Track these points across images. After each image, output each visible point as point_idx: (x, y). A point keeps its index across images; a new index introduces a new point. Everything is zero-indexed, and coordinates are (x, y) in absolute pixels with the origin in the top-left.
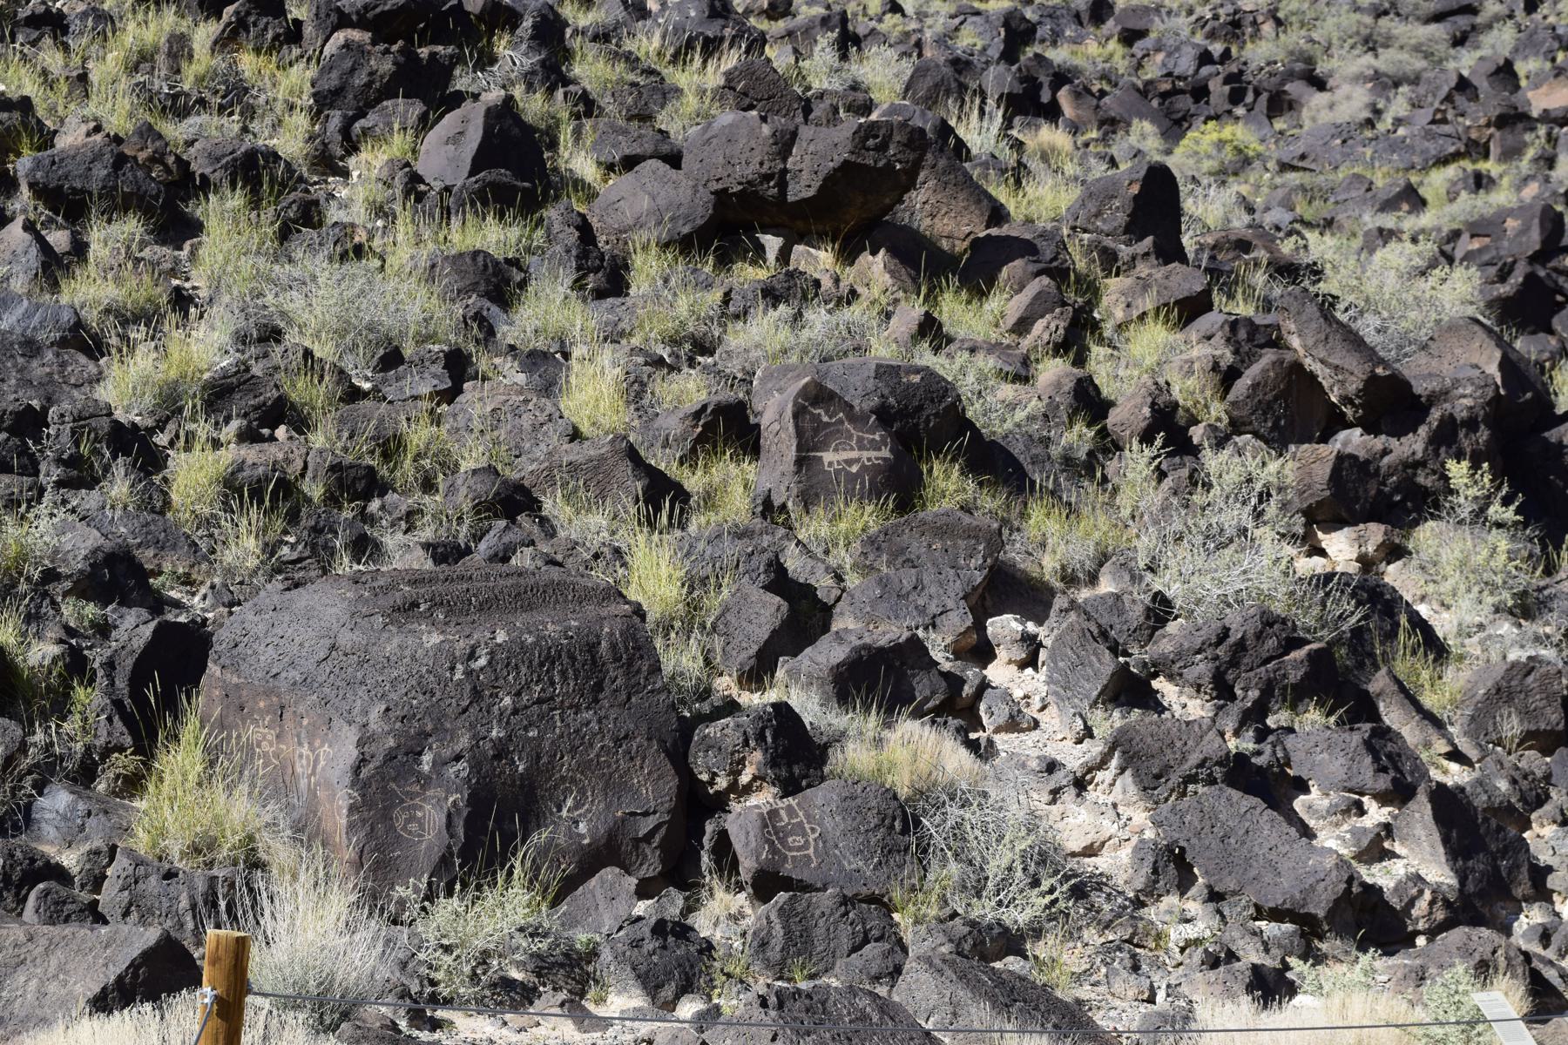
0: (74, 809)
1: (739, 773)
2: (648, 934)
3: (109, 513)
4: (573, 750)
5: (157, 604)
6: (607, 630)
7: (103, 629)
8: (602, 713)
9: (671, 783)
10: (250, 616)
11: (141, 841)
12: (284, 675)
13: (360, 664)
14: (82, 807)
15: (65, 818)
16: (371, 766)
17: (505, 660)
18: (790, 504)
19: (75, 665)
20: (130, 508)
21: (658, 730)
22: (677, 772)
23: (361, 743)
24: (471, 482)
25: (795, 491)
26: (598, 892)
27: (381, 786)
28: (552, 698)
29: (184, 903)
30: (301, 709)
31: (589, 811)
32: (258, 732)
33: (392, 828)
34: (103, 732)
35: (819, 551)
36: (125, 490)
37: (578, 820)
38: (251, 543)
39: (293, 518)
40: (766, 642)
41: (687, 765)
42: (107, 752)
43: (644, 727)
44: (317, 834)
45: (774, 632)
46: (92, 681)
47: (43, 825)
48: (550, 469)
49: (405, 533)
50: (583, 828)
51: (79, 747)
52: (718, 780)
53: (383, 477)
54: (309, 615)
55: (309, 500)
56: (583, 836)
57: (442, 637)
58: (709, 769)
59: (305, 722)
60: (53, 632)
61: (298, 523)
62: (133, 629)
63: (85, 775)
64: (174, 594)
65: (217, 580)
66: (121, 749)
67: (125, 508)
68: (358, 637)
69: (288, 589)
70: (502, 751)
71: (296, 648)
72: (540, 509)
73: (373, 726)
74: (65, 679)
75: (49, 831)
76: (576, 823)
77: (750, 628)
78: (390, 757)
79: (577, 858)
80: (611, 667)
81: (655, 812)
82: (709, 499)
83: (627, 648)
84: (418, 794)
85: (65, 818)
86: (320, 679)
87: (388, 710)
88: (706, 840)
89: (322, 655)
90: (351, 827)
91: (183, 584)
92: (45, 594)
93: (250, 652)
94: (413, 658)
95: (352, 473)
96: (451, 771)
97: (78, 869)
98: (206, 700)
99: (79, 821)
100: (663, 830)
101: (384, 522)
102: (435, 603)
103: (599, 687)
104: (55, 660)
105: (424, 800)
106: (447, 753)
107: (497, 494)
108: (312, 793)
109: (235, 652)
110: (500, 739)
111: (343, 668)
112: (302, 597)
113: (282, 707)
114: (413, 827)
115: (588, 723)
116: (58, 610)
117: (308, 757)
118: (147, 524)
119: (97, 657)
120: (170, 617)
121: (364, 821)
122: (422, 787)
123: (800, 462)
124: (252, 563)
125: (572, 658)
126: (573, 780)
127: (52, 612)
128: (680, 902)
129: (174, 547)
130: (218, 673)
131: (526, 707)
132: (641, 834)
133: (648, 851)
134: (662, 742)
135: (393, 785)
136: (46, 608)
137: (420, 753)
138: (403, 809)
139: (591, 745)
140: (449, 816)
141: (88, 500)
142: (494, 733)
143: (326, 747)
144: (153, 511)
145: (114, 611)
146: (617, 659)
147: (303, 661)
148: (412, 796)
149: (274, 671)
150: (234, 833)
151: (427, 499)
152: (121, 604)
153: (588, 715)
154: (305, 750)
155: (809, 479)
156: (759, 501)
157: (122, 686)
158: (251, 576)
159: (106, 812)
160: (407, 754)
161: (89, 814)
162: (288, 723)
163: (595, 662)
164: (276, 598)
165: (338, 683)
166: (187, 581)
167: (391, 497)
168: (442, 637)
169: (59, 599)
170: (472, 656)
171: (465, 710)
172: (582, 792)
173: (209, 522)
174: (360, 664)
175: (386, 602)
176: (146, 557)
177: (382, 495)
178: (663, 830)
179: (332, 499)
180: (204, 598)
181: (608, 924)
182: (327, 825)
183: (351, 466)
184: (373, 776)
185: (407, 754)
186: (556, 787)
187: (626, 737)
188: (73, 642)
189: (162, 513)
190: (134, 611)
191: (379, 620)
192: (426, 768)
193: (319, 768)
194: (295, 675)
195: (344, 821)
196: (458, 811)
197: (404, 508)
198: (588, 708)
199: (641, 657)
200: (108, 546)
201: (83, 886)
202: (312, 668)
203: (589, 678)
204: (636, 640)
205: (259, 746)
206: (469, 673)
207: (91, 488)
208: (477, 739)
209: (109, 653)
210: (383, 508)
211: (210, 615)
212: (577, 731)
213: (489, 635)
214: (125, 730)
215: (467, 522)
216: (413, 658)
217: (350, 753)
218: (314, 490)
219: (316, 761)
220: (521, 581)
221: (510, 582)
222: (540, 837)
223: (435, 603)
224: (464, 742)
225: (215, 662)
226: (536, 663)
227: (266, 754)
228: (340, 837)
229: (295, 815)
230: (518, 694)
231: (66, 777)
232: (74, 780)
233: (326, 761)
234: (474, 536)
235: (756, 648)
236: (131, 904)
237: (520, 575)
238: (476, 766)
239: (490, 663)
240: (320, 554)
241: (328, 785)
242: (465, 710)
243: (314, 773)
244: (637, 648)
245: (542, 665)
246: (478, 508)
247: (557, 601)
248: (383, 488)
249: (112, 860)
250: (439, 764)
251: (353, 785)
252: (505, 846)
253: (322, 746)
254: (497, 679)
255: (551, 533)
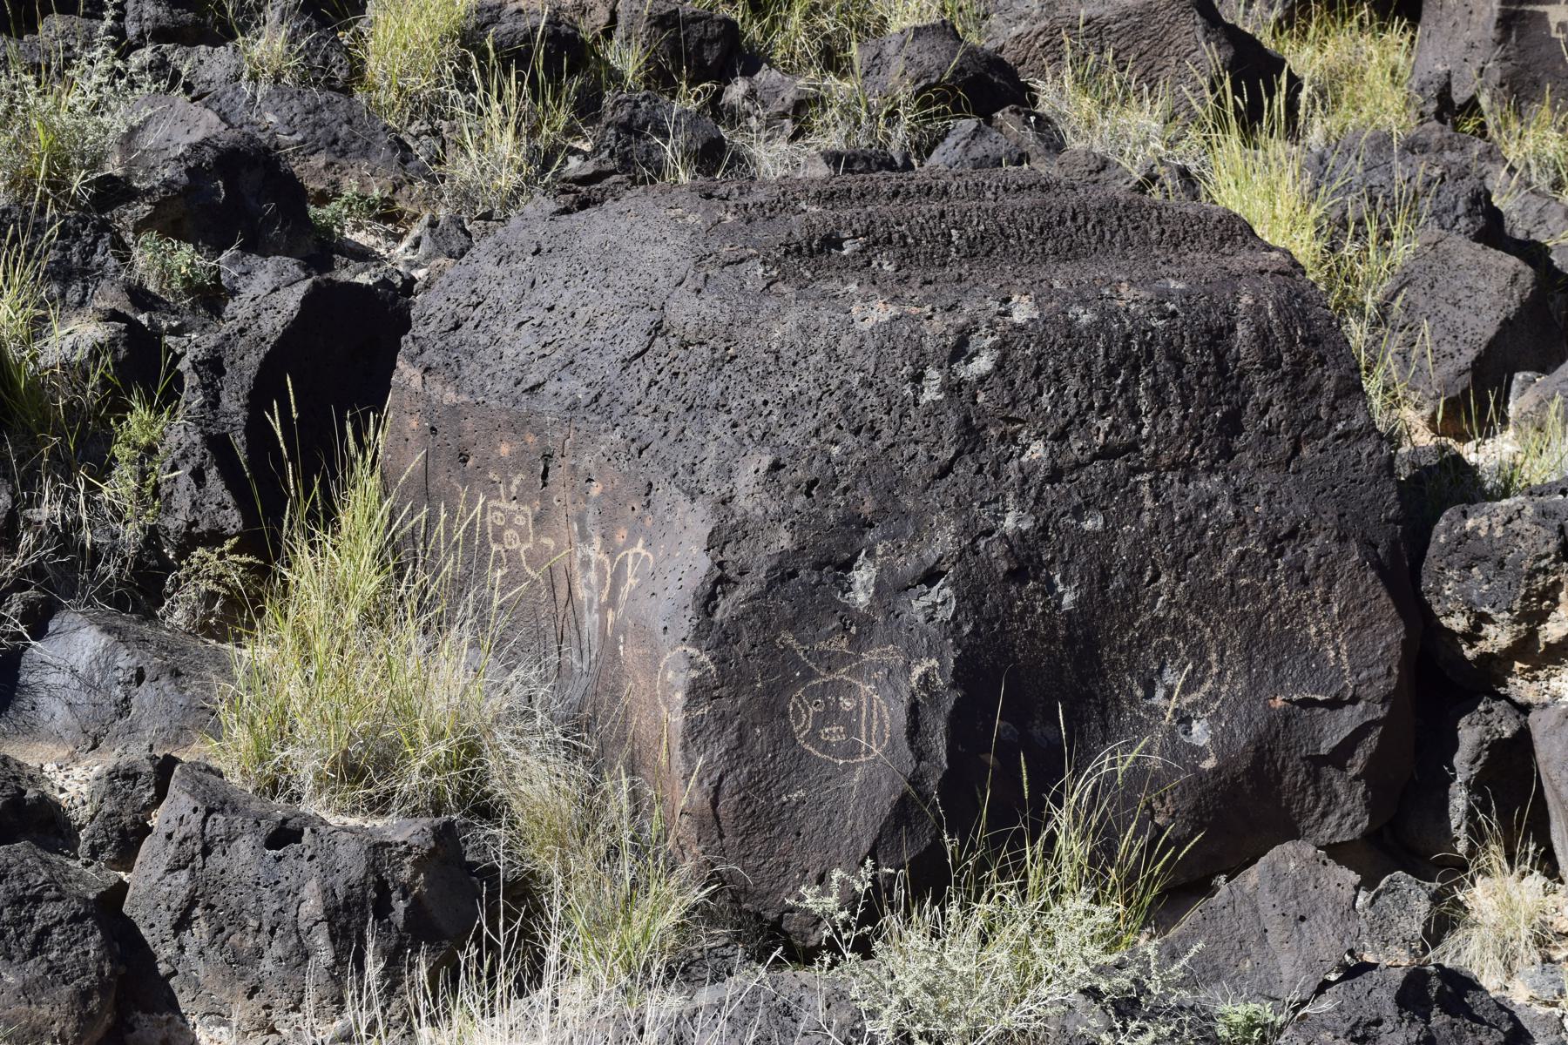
0: (110, 666)
1: (1543, 617)
2: (1390, 1010)
3: (246, 87)
4: (1180, 562)
5: (320, 250)
6: (1246, 300)
7: (211, 297)
8: (1241, 481)
9: (1389, 635)
10: (488, 267)
11: (230, 755)
12: (551, 387)
13: (716, 365)
14: (125, 661)
15: (89, 685)
16: (740, 593)
17: (1034, 360)
18: (1484, 101)
19: (139, 363)
20: (286, 80)
21: (1358, 518)
22: (1403, 613)
23: (716, 542)
24: (911, 49)
25: (1497, 76)
26: (1266, 901)
27: (762, 638)
28: (1133, 447)
29: (311, 905)
30: (587, 462)
31: (1213, 695)
32: (503, 512)
33: (787, 735)
34: (182, 502)
35: (1544, 183)
36: (279, 46)
37: (1187, 719)
38: (506, 144)
39: (588, 107)
40: (1492, 343)
41: (1419, 595)
42: (190, 541)
43: (1330, 514)
44: (621, 741)
45: (1506, 323)
46: (171, 395)
47: (43, 699)
48: (1052, 32)
49: (794, 138)
50: (1200, 733)
51: (130, 534)
52: (1489, 629)
53: (751, 44)
54: (607, 261)
55: (617, 77)
56: (1200, 753)
57: (893, 310)
58: (1471, 607)
59: (595, 490)
60: (109, 296)
61: (596, 119)
62: (269, 293)
63: (140, 590)
64: (362, 238)
65: (442, 213)
66: (215, 538)
67: (278, 77)
68: (709, 307)
69: (567, 211)
70: (1026, 563)
71: (579, 331)
72: (1034, 101)
73: (743, 503)
74: (116, 391)
75: (54, 711)
76: (1185, 720)
77: (1458, 316)
78: (783, 573)
79: (1188, 803)
80: (1257, 380)
81: (1354, 700)
82: (1327, 95)
83: (1291, 341)
84: (844, 659)
85: (89, 685)
86: (629, 397)
87: (776, 466)
88: (1461, 759)
89: (634, 346)
90: (694, 733)
91: (378, 218)
92: (104, 226)
93: (484, 339)
94: (832, 354)
95: (697, 31)
96: (917, 605)
97: (89, 810)
98: (398, 434)
99: (118, 692)
100: (1372, 740)
101: (753, 122)
102: (876, 240)
103: (1233, 424)
104: (95, 354)
105: (857, 672)
106: (907, 565)
107: (959, 71)
108: (609, 645)
109: (454, 339)
110: (1022, 535)
111: (679, 372)
112: (595, 226)
113: (547, 457)
114: (834, 733)
115: (1213, 501)
116: (123, 252)
117: (600, 567)
118: (317, 108)
119: (189, 348)
120: (343, 276)
121: (723, 720)
122: (853, 641)
123: (1507, 22)
124: (508, 179)
125: (1177, 359)
126: (1179, 628)
127: (113, 262)
128: (1422, 907)
129: (366, 151)
130: (416, 382)
131: (1079, 466)
132: (1325, 748)
133: (1339, 786)
134: (1368, 544)
135: (789, 638)
136: (103, 256)
137: (848, 566)
138: (811, 693)
139: (1218, 550)
140: (914, 709)
141: (212, 64)
142: (1009, 522)
143: (639, 548)
144: (330, 84)
145: (233, 262)
146: (1271, 364)
147: (592, 359)
148: (831, 661)
149: (531, 379)
150: (436, 736)
151: (831, 80)
152: (246, 249)
153: (1210, 484)
154: (595, 551)
155: (1522, 52)
156: (1431, 92)
157: (234, 407)
158: (506, 206)
159: (176, 674)
160: (818, 566)
161: (140, 677)
162: (560, 491)
163: (1223, 370)
164: (540, 230)
165: (667, 406)
166: (388, 215)
167: (764, 76)
168: (893, 310)
169: (129, 238)
170: (961, 350)
171: (945, 471)
172: (1199, 653)
173: (434, 108)
174: (716, 365)
175: (770, 235)
176: (311, 171)
177: (749, 72)
178: (1372, 740)
179: (660, 78)
180: (416, 244)
181: (1293, 977)
182: (640, 723)
183: (696, 19)
184: (743, 617)
185: (818, 566)
186: (1142, 642)
187: (1292, 534)
188: (143, 318)
189: (347, 91)
190: (272, 263)
191: (756, 272)
192: (861, 598)
193: (625, 592)
194: (575, 387)
195: (677, 720)
196: (934, 696)
197: (790, 96)
198: (1210, 470)
199: (1322, 361)
200: (227, 137)
201: (95, 852)
202: (613, 373)
203: (1211, 405)
204: (1309, 325)
205: (498, 538)
206: (953, 388)
207: (216, 42)
208: (974, 534)
209: (212, 340)
210: (751, 95)
211: (420, 274)
212: (1188, 520)
213: (996, 307)
214: (228, 498)
215: (905, 120)
216: (832, 354)
217: (695, 564)
218: (627, 59)
219: (618, 577)
220: (1049, 198)
221: (1027, 201)
222: (1114, 761)
223: (876, 240)
224: (944, 540)
225: (412, 359)
226: (1099, 366)
227: (512, 556)
228: (668, 754)
229: (574, 692)
230: (1061, 436)
231: (103, 594)
232: (120, 603)
233: (640, 578)
234: (918, 147)
235: (1470, 354)
236: (192, 902)
237: (1046, 188)
238: (971, 595)
239: (999, 366)
240: (633, 164)
241: (642, 632)
242: (945, 471)
243: (612, 602)
244: (1313, 341)
245: (1111, 372)
246: (924, 97)
247: (1127, 242)
248: (752, 62)
249: (161, 794)
250: (890, 590)
251: (699, 636)
252: (1039, 787)
253: (631, 543)
254: (1014, 402)
255: (1056, 146)
